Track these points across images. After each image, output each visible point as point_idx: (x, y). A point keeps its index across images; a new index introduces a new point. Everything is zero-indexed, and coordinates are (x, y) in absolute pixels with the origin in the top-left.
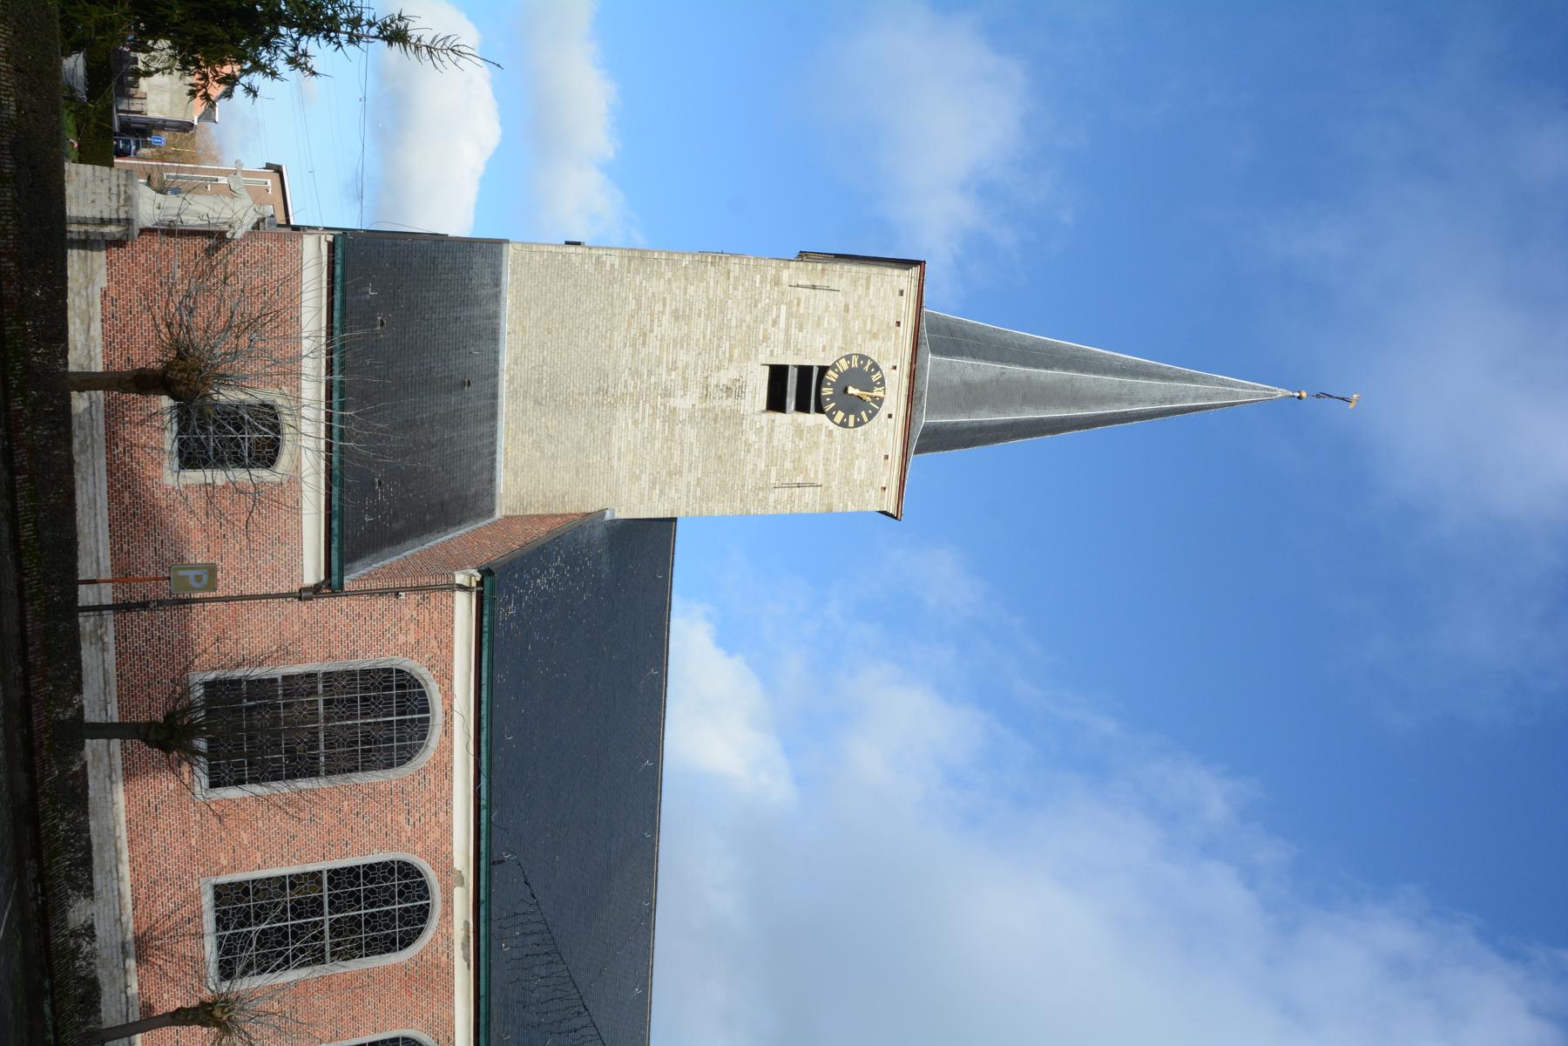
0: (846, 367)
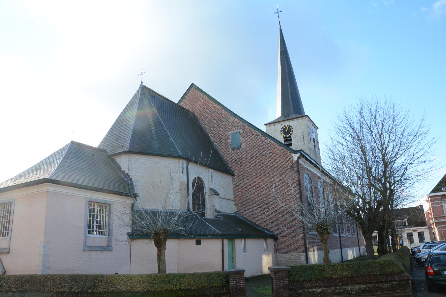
0: (285, 135)
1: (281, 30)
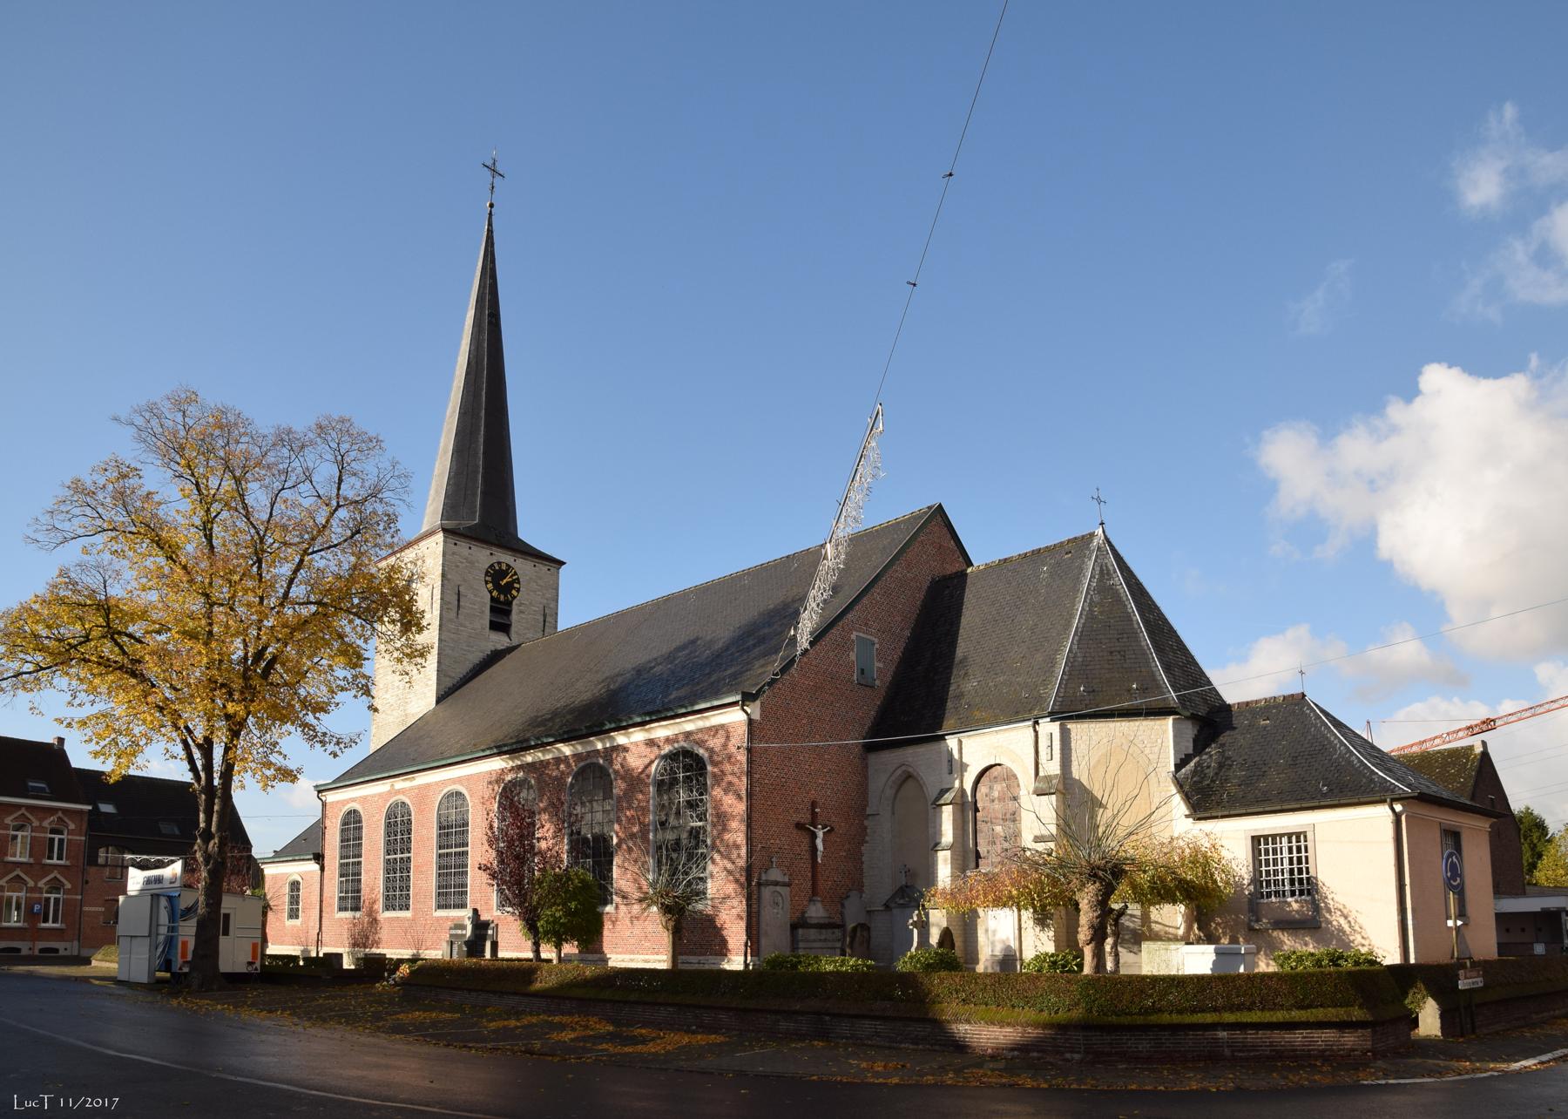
1: (490, 232)
